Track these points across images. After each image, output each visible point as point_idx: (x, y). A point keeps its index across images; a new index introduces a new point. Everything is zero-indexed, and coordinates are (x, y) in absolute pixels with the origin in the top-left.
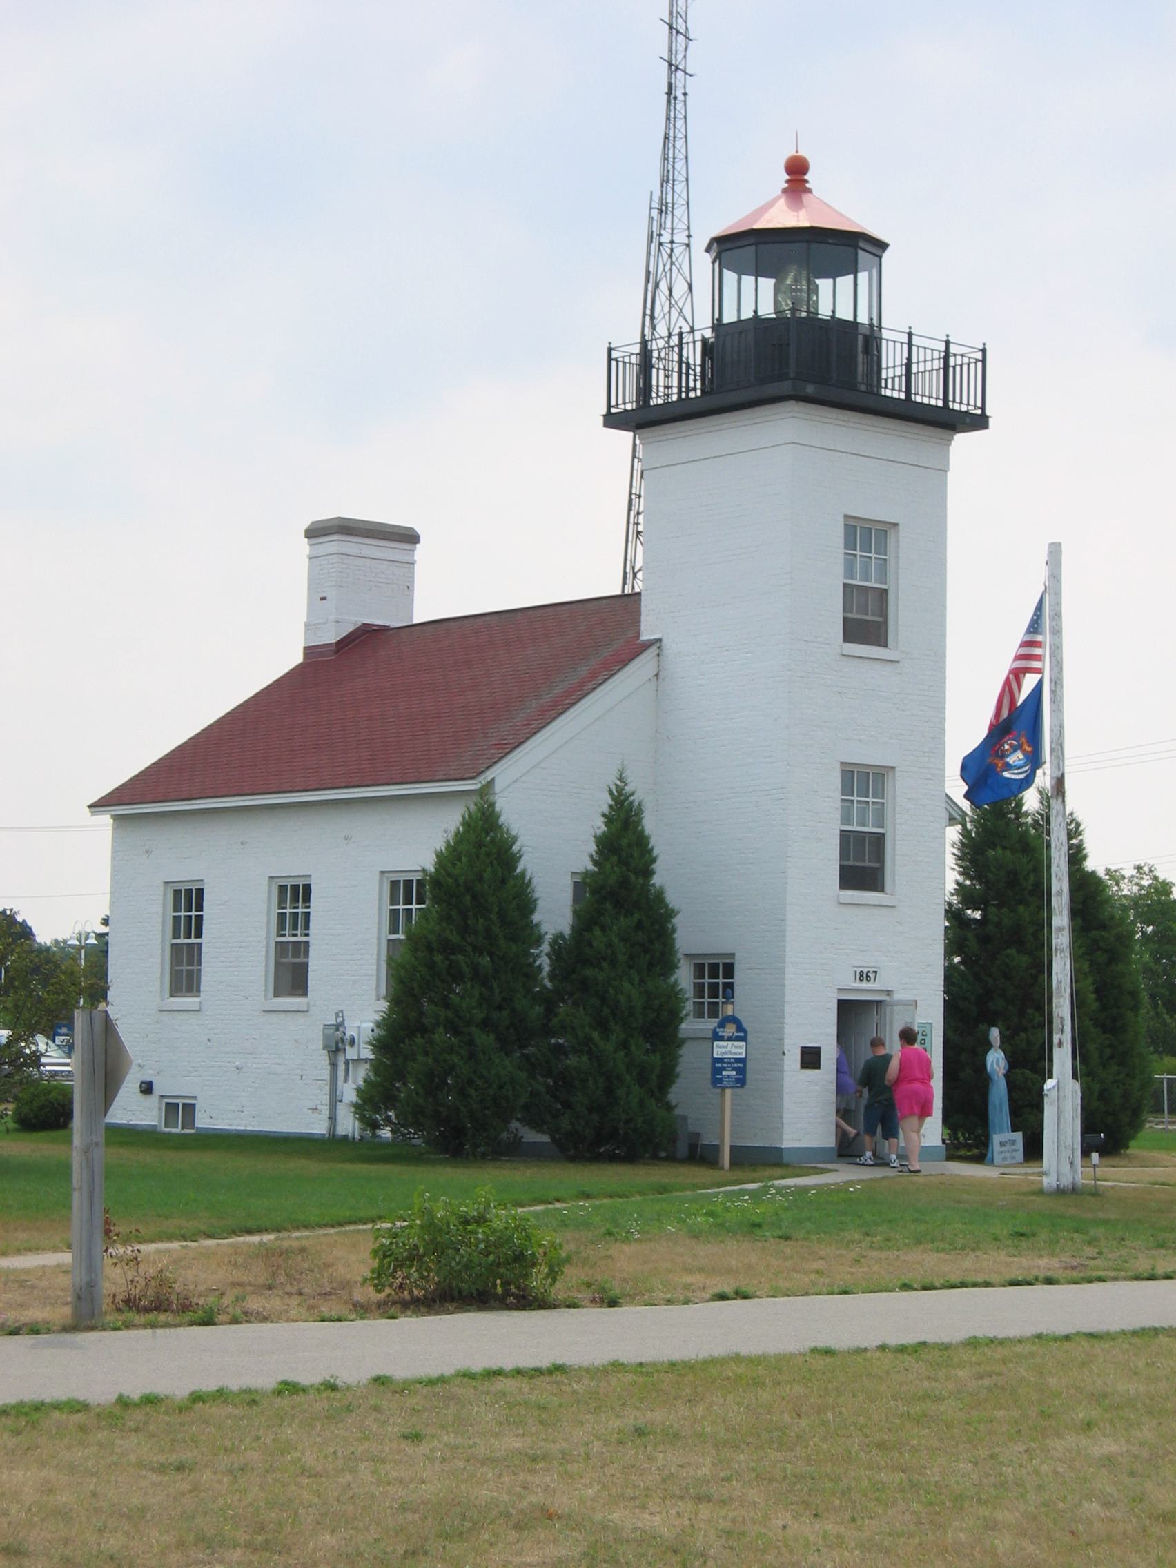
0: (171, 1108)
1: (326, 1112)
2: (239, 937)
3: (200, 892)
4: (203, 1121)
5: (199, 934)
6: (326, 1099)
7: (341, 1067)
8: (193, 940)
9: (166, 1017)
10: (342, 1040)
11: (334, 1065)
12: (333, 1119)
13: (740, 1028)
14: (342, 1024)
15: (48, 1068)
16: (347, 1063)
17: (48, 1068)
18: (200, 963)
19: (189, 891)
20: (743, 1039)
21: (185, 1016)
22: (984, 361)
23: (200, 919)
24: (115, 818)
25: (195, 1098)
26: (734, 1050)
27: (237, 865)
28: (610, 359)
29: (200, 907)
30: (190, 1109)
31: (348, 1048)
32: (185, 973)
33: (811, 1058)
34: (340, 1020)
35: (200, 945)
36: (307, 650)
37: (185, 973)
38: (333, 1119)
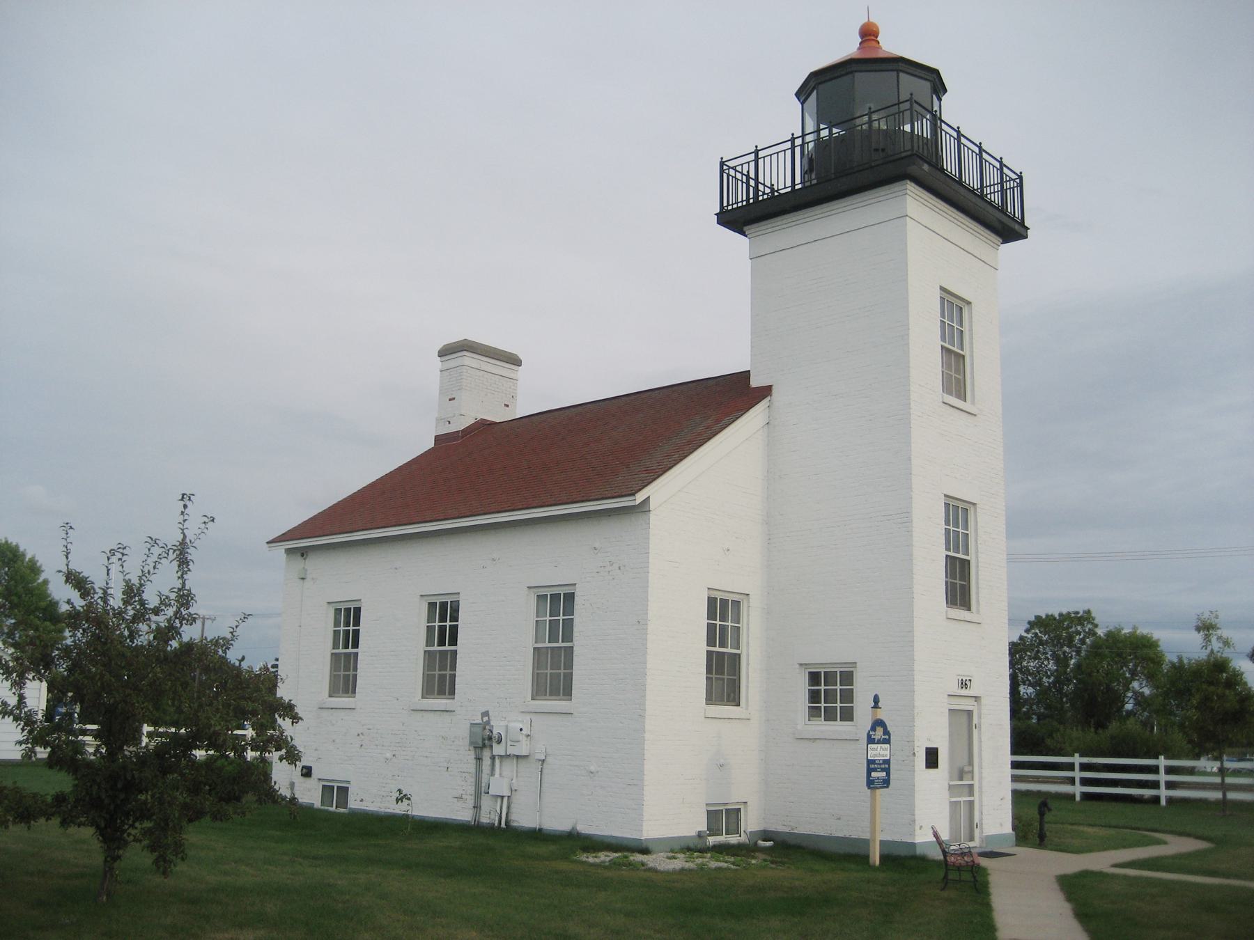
0: (327, 790)
1: (470, 802)
2: (393, 645)
3: (358, 610)
4: (353, 803)
5: (356, 645)
6: (471, 790)
7: (487, 762)
8: (350, 650)
9: (325, 713)
10: (490, 738)
11: (479, 759)
12: (477, 807)
13: (886, 732)
14: (488, 722)
15: (798, 180)
16: (493, 758)
17: (798, 180)
18: (356, 669)
19: (348, 610)
20: (887, 741)
21: (342, 713)
22: (1021, 185)
23: (356, 633)
24: (289, 551)
25: (348, 782)
26: (882, 752)
27: (393, 585)
28: (722, 171)
29: (357, 623)
30: (344, 791)
31: (494, 745)
32: (344, 677)
33: (932, 758)
34: (485, 719)
35: (356, 654)
36: (438, 439)
37: (344, 677)
38: (477, 807)
